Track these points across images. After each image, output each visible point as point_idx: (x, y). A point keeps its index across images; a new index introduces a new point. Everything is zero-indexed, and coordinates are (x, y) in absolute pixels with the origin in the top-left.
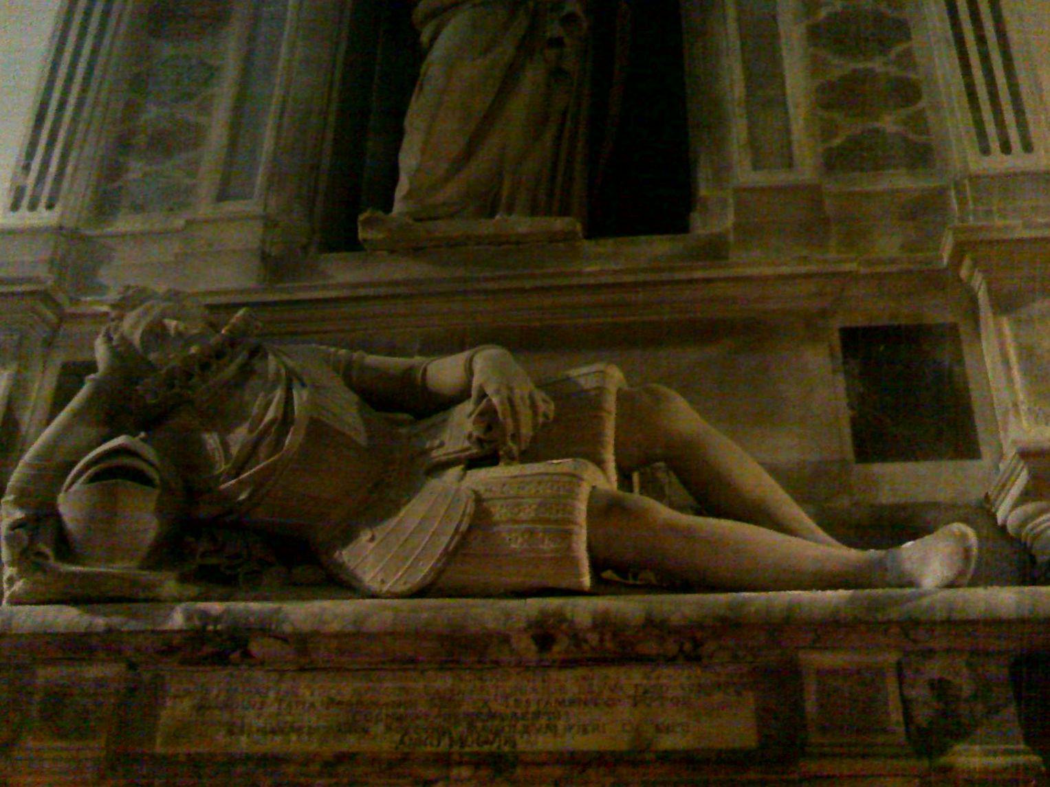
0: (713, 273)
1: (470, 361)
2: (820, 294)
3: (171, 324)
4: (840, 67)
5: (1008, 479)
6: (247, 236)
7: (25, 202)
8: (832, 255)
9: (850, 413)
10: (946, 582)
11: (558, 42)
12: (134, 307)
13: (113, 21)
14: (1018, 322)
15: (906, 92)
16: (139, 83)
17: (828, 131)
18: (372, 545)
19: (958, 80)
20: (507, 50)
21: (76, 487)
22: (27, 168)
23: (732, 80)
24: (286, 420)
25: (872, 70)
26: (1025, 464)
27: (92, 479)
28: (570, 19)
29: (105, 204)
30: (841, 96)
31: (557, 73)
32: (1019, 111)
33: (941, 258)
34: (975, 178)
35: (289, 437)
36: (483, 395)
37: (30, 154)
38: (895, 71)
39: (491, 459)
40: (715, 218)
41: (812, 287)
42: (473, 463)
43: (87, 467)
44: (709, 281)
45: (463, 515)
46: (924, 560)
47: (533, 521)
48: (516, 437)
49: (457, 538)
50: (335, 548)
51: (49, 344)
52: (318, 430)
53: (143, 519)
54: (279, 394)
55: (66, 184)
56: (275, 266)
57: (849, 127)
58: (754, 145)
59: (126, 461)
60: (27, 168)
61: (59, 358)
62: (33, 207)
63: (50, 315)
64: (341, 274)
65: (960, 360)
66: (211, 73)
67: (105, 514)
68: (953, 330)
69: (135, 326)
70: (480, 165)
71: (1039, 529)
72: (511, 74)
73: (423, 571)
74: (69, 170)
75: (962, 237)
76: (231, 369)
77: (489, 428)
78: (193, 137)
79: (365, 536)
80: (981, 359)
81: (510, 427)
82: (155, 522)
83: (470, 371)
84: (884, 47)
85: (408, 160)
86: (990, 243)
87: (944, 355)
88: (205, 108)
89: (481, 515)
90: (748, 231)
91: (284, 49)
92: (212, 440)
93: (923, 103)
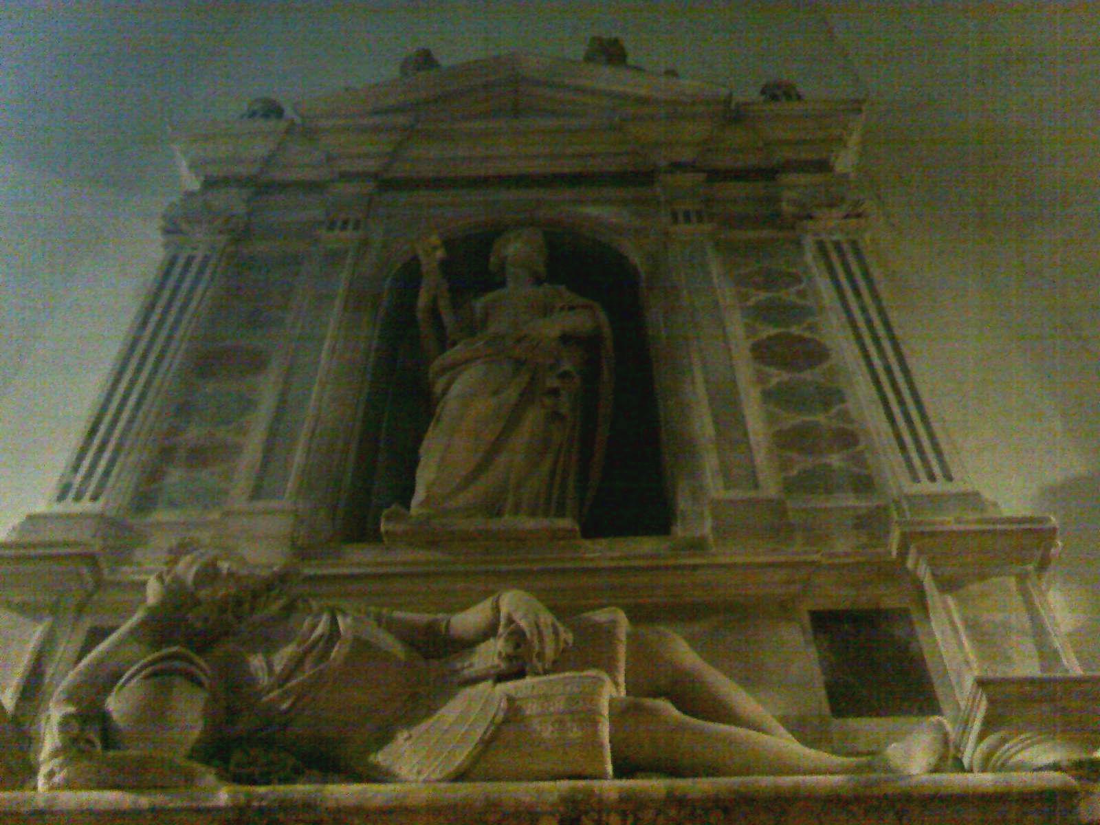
0: (697, 561)
1: (497, 601)
2: (789, 582)
3: (224, 566)
4: (792, 420)
5: (969, 716)
6: (280, 525)
7: (71, 495)
8: (797, 548)
9: (823, 678)
10: (931, 768)
11: (554, 392)
12: (187, 553)
13: (165, 364)
14: (962, 602)
15: (847, 439)
16: (184, 410)
17: (784, 466)
18: (408, 743)
19: (885, 426)
20: (511, 394)
21: (133, 682)
22: (76, 469)
23: (703, 425)
24: (333, 635)
25: (817, 424)
26: (983, 690)
27: (147, 677)
28: (564, 376)
29: (144, 501)
30: (792, 441)
31: (555, 416)
32: (939, 454)
33: (890, 553)
34: (909, 498)
35: (336, 648)
36: (510, 621)
37: (80, 458)
38: (835, 424)
39: (520, 674)
40: (696, 521)
41: (780, 575)
42: (501, 678)
43: (145, 666)
44: (695, 567)
45: (498, 709)
46: (908, 755)
47: (563, 713)
48: (540, 656)
49: (493, 728)
50: (368, 752)
51: (80, 610)
52: (362, 646)
53: (190, 715)
54: (325, 618)
55: (111, 480)
56: (303, 553)
57: (802, 463)
58: (726, 473)
59: (177, 664)
60: (76, 469)
61: (88, 623)
62: (78, 498)
63: (88, 577)
64: (360, 558)
65: (912, 633)
66: (248, 404)
67: (154, 712)
68: (904, 614)
69: (190, 565)
70: (484, 484)
71: (1004, 757)
72: (513, 420)
73: (460, 758)
74: (115, 471)
75: (907, 529)
76: (274, 608)
77: (518, 646)
78: (230, 451)
79: (402, 736)
80: (931, 634)
81: (537, 649)
82: (200, 725)
83: (497, 609)
84: (827, 405)
85: (425, 476)
86: (933, 534)
87: (899, 631)
88: (243, 431)
89: (514, 711)
90: (723, 532)
91: (316, 388)
92: (256, 662)
93: (860, 447)
